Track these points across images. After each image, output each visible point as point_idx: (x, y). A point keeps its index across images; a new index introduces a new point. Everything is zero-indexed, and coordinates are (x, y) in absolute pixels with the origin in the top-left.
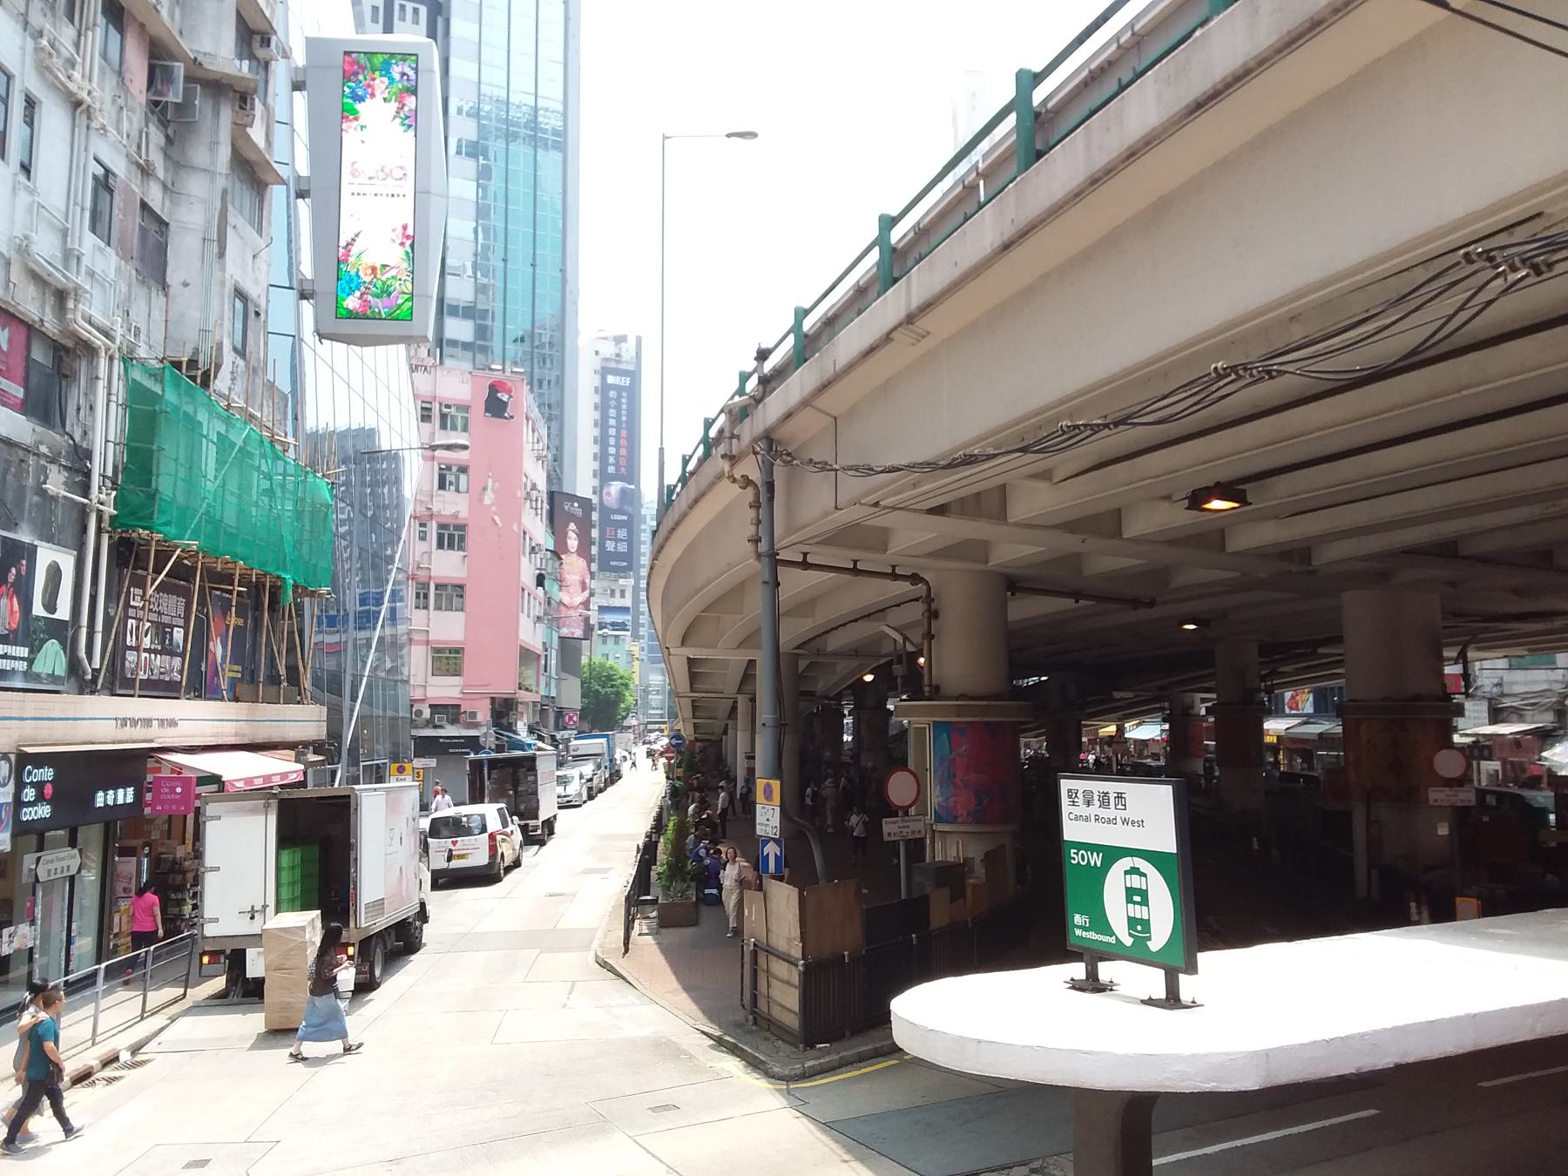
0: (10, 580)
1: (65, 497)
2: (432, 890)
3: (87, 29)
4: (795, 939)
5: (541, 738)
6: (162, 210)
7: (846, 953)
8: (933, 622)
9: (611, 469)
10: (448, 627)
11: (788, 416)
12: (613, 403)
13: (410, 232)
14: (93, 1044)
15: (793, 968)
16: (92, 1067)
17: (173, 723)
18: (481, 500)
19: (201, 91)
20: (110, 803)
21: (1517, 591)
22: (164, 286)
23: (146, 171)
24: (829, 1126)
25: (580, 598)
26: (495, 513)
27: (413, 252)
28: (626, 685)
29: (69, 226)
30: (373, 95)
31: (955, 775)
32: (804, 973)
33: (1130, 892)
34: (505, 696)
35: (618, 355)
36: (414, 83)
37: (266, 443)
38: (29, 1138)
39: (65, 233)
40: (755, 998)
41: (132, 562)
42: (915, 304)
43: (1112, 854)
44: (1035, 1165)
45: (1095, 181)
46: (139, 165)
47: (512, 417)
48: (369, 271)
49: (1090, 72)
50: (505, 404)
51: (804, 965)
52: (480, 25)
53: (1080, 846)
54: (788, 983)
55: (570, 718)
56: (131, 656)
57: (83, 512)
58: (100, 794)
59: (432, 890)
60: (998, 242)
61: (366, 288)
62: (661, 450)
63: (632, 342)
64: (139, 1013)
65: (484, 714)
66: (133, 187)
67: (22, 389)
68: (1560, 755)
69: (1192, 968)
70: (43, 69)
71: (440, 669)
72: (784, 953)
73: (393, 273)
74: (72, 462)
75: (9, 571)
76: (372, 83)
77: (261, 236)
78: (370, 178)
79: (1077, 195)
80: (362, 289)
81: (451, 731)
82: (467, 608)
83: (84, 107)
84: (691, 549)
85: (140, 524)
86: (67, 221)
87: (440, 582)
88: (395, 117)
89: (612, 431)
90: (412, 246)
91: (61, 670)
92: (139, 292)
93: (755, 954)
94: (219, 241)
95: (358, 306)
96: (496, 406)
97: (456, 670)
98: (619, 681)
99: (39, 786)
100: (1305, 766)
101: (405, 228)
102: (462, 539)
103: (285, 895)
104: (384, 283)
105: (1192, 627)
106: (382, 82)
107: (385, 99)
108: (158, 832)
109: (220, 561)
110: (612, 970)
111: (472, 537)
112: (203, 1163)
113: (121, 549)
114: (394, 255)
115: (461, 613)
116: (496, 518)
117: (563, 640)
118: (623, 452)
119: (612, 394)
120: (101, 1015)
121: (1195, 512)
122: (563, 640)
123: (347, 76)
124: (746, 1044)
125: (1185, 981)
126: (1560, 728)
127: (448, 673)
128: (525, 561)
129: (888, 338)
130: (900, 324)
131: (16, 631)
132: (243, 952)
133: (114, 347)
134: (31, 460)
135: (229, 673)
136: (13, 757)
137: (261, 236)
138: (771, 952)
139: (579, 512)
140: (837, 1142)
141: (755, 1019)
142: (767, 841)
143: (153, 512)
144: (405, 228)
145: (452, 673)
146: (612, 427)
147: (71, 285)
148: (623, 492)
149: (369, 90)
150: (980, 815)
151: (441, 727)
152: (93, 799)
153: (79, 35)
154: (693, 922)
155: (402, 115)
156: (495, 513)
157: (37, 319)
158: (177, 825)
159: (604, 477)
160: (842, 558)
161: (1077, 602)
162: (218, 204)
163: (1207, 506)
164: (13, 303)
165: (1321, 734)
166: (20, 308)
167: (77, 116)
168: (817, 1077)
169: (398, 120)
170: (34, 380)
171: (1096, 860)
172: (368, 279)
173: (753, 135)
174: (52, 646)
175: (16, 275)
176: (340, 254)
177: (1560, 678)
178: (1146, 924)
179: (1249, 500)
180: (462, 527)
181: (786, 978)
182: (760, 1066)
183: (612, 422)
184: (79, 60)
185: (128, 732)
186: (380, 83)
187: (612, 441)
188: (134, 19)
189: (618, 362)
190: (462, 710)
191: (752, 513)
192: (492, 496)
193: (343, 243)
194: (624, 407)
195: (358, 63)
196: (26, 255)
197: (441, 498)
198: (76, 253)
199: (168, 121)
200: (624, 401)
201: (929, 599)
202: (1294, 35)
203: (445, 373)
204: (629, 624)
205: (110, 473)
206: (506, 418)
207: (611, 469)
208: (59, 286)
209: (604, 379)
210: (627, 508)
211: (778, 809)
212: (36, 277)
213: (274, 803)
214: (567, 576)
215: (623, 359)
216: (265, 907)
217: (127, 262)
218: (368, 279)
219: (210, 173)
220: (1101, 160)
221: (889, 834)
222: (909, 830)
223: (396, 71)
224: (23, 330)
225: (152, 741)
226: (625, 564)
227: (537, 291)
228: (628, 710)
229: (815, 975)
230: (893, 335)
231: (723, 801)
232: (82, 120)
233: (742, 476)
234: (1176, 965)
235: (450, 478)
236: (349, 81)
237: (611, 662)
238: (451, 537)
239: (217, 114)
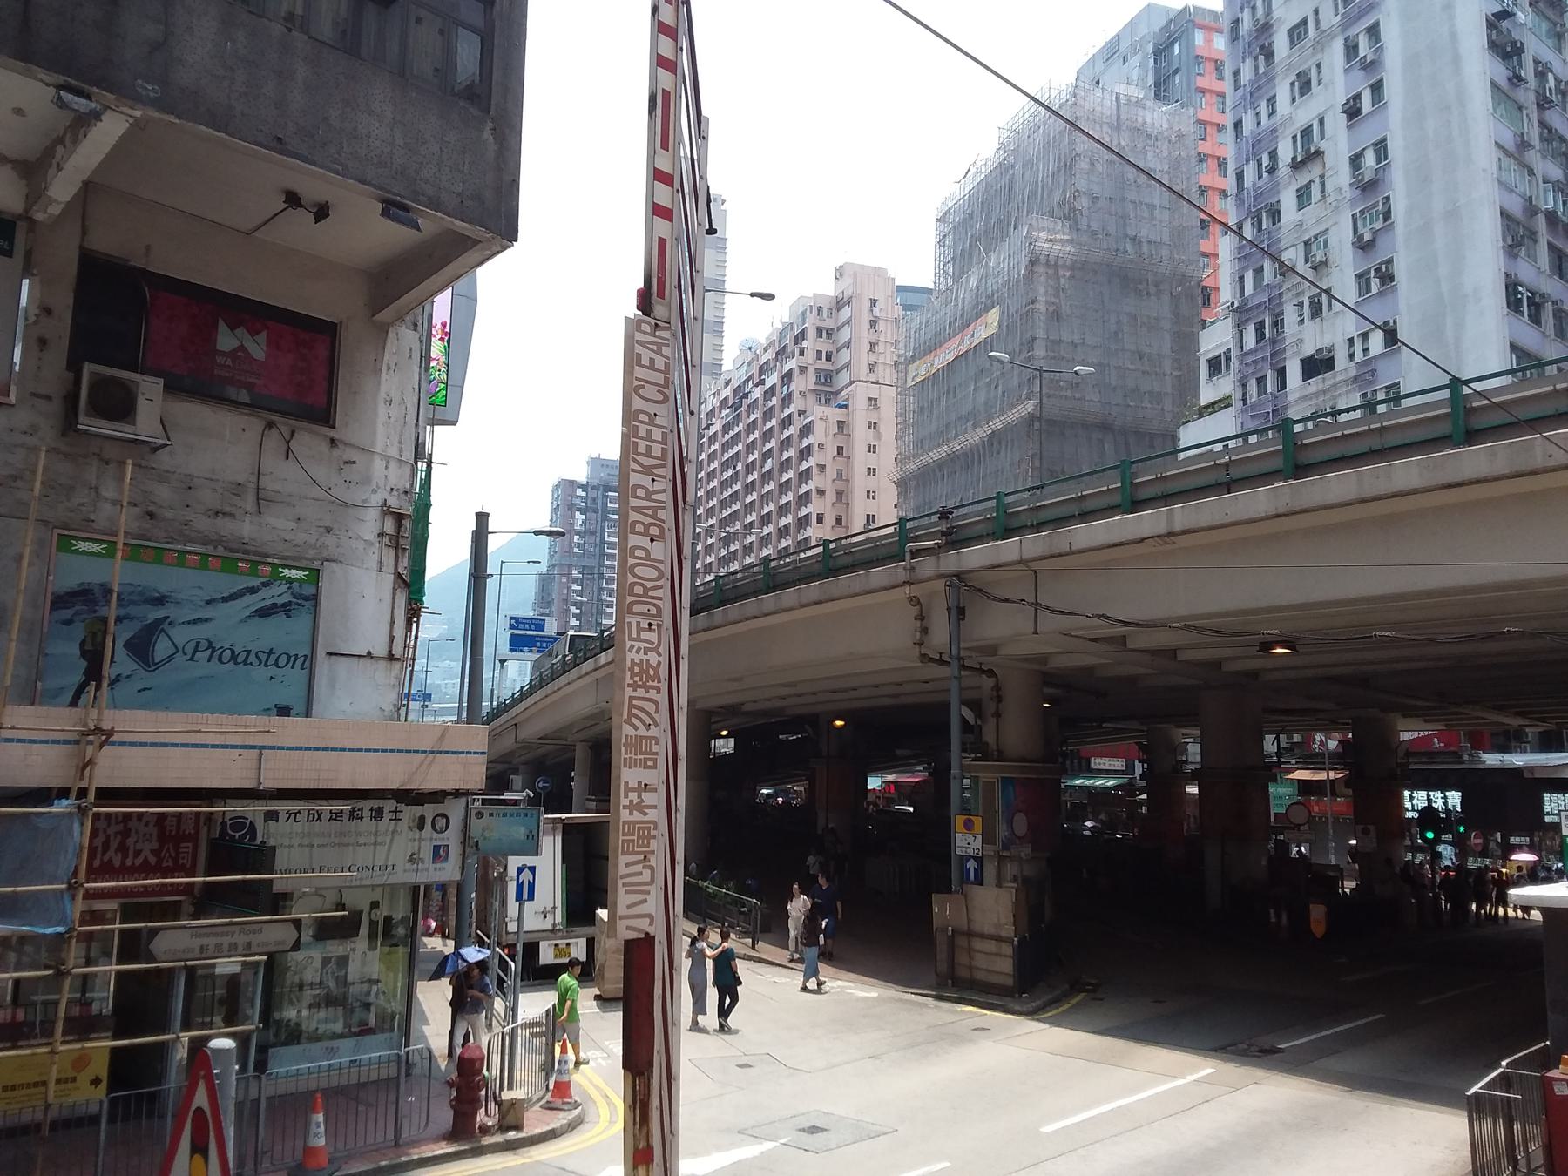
24: (1094, 1033)
60: (1273, 512)
93: (951, 940)
105: (1047, 705)
129: (1142, 540)
132: (538, 943)
138: (970, 934)
211: (979, 838)
213: (560, 826)
216: (554, 907)
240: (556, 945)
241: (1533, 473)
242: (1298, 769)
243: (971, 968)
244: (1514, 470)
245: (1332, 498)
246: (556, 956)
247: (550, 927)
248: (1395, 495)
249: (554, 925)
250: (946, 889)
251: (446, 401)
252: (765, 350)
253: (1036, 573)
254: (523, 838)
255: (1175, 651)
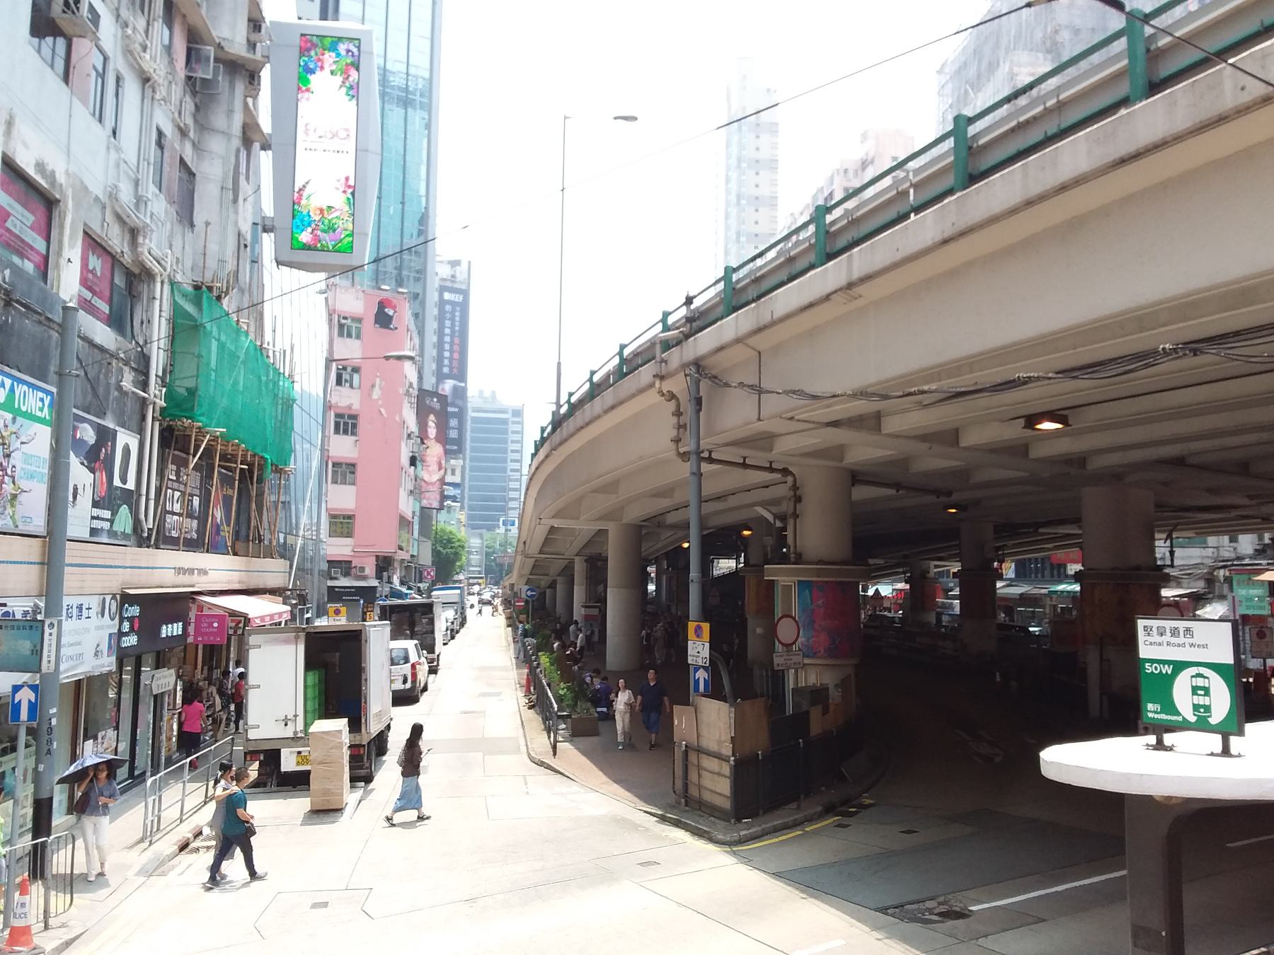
0: (102, 458)
1: (133, 392)
2: (393, 706)
3: (154, 20)
4: (725, 741)
5: (409, 588)
6: (192, 163)
7: (760, 753)
8: (798, 505)
9: (446, 370)
10: (343, 498)
11: (721, 349)
12: (448, 315)
13: (351, 182)
14: (181, 822)
15: (724, 764)
16: (189, 839)
17: (203, 572)
18: (370, 395)
19: (224, 72)
20: (170, 635)
21: (1211, 491)
22: (192, 225)
23: (183, 133)
24: (778, 875)
25: (436, 477)
26: (381, 406)
27: (354, 198)
28: (463, 547)
29: (140, 177)
30: (322, 68)
31: (814, 622)
32: (735, 766)
33: (1195, 690)
34: (387, 555)
35: (453, 276)
36: (356, 58)
37: (258, 348)
38: (223, 877)
39: (137, 183)
40: (686, 786)
41: (173, 444)
42: (856, 275)
43: (1179, 666)
44: (941, 899)
45: (1029, 203)
46: (180, 128)
47: (396, 328)
48: (318, 212)
49: (1019, 123)
50: (391, 318)
51: (734, 761)
52: (364, 4)
53: (1152, 661)
54: (719, 774)
55: (428, 573)
56: (169, 518)
57: (143, 403)
58: (164, 627)
59: (393, 706)
60: (939, 238)
61: (317, 225)
62: (559, 364)
63: (464, 265)
64: (203, 799)
65: (370, 570)
66: (176, 145)
67: (108, 307)
68: (1209, 613)
69: (1241, 733)
70: (128, 52)
71: (336, 531)
72: (715, 752)
73: (337, 214)
74: (139, 365)
75: (101, 450)
76: (321, 57)
77: (248, 183)
78: (320, 137)
79: (1013, 211)
80: (313, 226)
81: (344, 582)
82: (358, 481)
83: (150, 83)
84: (592, 443)
85: (183, 414)
86: (138, 172)
87: (335, 460)
88: (341, 87)
89: (447, 339)
90: (353, 194)
91: (129, 530)
92: (178, 228)
93: (686, 753)
94: (233, 189)
95: (310, 240)
96: (383, 320)
97: (348, 533)
98: (458, 544)
99: (131, 619)
100: (1007, 618)
101: (347, 179)
102: (354, 426)
103: (310, 708)
104: (330, 221)
105: (954, 511)
106: (330, 56)
107: (332, 73)
108: (176, 659)
109: (230, 444)
110: (549, 767)
111: (363, 425)
112: (325, 905)
113: (165, 434)
114: (339, 200)
115: (353, 486)
116: (382, 410)
117: (422, 508)
118: (456, 356)
119: (448, 308)
120: (186, 798)
121: (1029, 431)
122: (422, 508)
123: (304, 51)
124: (688, 819)
125: (1234, 740)
126: (1209, 593)
127: (342, 535)
128: (403, 445)
129: (827, 298)
130: (840, 289)
131: (103, 498)
132: (278, 751)
133: (165, 274)
134: (114, 362)
135: (227, 533)
136: (118, 597)
137: (248, 183)
138: (700, 751)
139: (437, 406)
140: (790, 885)
141: (686, 801)
142: (697, 668)
143: (194, 406)
144: (347, 179)
145: (345, 535)
146: (447, 335)
147: (141, 225)
148: (455, 388)
149: (319, 64)
150: (834, 651)
151: (336, 579)
152: (159, 632)
153: (148, 24)
154: (594, 733)
155: (347, 84)
156: (381, 406)
157: (119, 251)
158: (190, 655)
159: (441, 377)
160: (734, 455)
161: (938, 497)
162: (233, 160)
163: (1039, 427)
164: (106, 238)
165: (1021, 595)
166: (110, 242)
167: (146, 90)
168: (750, 842)
169: (344, 89)
170: (115, 299)
171: (1168, 670)
172: (317, 218)
173: (635, 119)
174: (124, 510)
175: (109, 217)
176: (295, 198)
177: (1210, 554)
178: (1207, 708)
179: (1070, 423)
180: (354, 417)
181: (717, 771)
182: (705, 835)
183: (447, 331)
184: (149, 45)
185: (185, 579)
186: (329, 58)
187: (447, 347)
188: (179, 10)
189: (453, 282)
190: (353, 565)
191: (675, 420)
192: (380, 392)
193: (296, 189)
194: (457, 319)
195: (311, 41)
196: (114, 201)
197: (337, 393)
198: (145, 199)
199: (197, 92)
200: (457, 314)
201: (795, 487)
202: (1203, 124)
203: (343, 291)
204: (459, 497)
205: (160, 374)
206: (391, 329)
207: (446, 370)
208: (132, 225)
209: (441, 296)
210: (459, 402)
211: (707, 645)
212: (119, 218)
213: (302, 635)
214: (428, 458)
215: (458, 280)
216: (296, 716)
217: (171, 206)
218: (317, 218)
219: (227, 135)
220: (1035, 189)
221: (778, 665)
222: (792, 662)
223: (342, 48)
224: (110, 260)
225: (193, 586)
226: (456, 448)
227: (382, 219)
228: (461, 567)
229: (743, 769)
230: (834, 296)
231: (581, 642)
232: (148, 92)
233: (668, 391)
234: (1228, 731)
235: (345, 376)
236: (304, 56)
237: (449, 528)
238: (346, 424)
239: (232, 87)
240: (299, 753)
241: (1222, 119)
242: (1268, 570)
243: (699, 786)
244: (1197, 121)
245: (997, 206)
246: (298, 763)
247: (291, 735)
248: (1063, 188)
249: (295, 733)
250: (686, 702)
251: (352, 247)
252: (802, 214)
253: (759, 352)
254: (28, 653)
255: (957, 431)
